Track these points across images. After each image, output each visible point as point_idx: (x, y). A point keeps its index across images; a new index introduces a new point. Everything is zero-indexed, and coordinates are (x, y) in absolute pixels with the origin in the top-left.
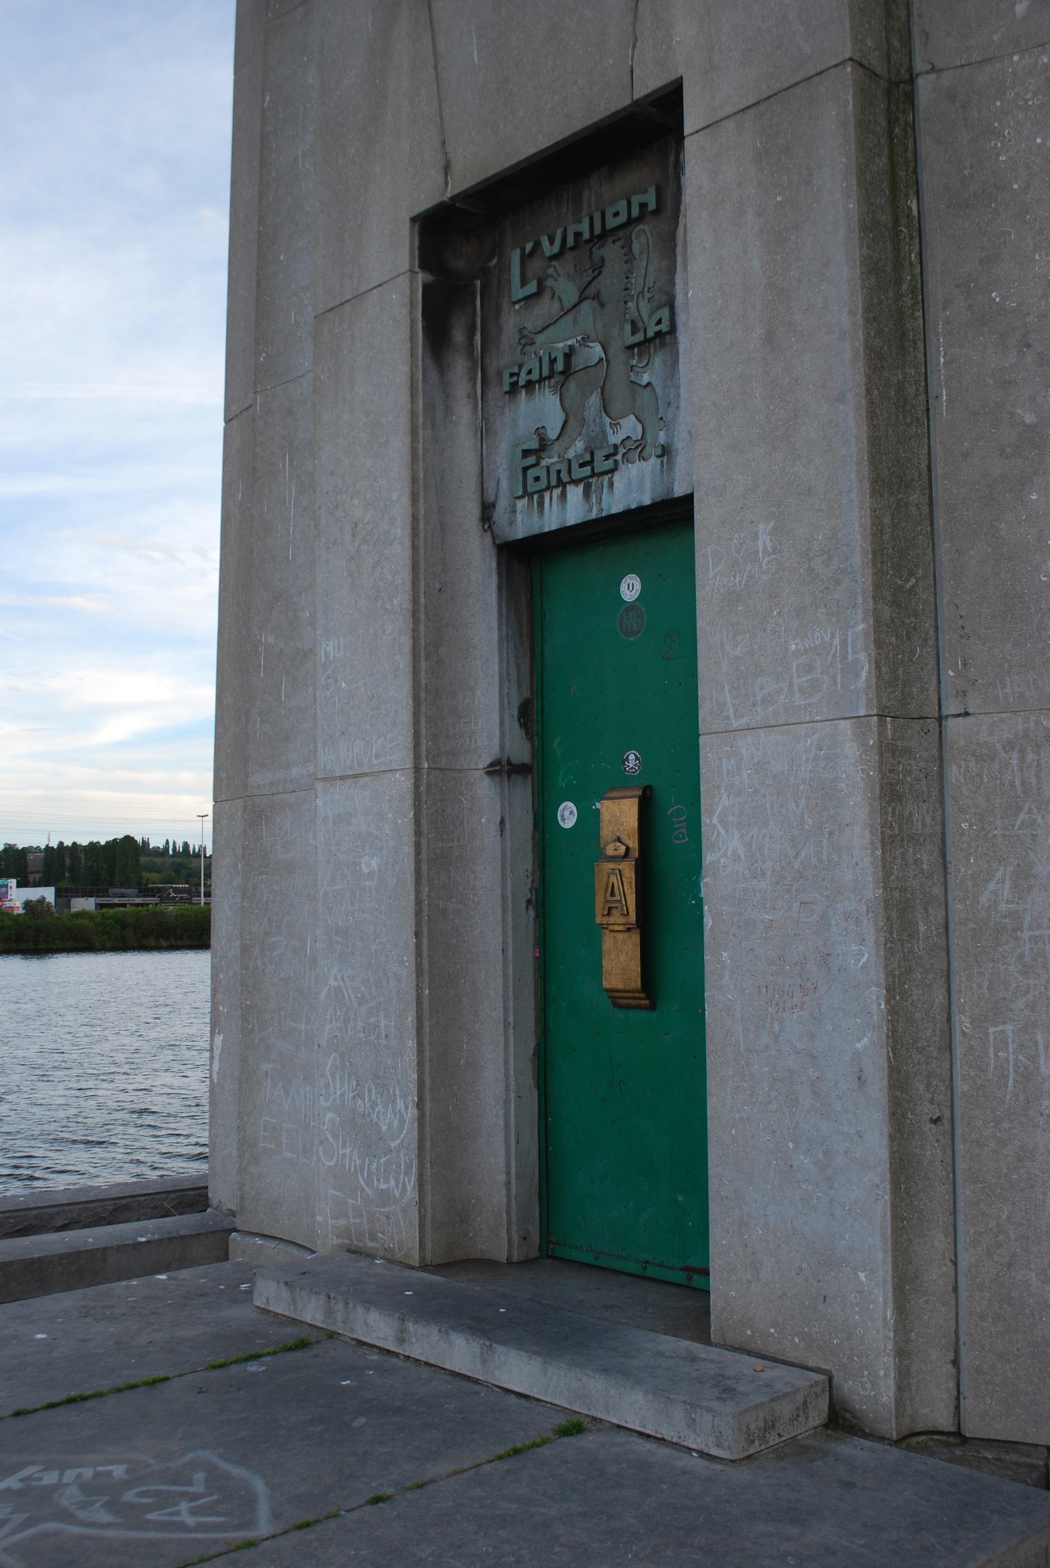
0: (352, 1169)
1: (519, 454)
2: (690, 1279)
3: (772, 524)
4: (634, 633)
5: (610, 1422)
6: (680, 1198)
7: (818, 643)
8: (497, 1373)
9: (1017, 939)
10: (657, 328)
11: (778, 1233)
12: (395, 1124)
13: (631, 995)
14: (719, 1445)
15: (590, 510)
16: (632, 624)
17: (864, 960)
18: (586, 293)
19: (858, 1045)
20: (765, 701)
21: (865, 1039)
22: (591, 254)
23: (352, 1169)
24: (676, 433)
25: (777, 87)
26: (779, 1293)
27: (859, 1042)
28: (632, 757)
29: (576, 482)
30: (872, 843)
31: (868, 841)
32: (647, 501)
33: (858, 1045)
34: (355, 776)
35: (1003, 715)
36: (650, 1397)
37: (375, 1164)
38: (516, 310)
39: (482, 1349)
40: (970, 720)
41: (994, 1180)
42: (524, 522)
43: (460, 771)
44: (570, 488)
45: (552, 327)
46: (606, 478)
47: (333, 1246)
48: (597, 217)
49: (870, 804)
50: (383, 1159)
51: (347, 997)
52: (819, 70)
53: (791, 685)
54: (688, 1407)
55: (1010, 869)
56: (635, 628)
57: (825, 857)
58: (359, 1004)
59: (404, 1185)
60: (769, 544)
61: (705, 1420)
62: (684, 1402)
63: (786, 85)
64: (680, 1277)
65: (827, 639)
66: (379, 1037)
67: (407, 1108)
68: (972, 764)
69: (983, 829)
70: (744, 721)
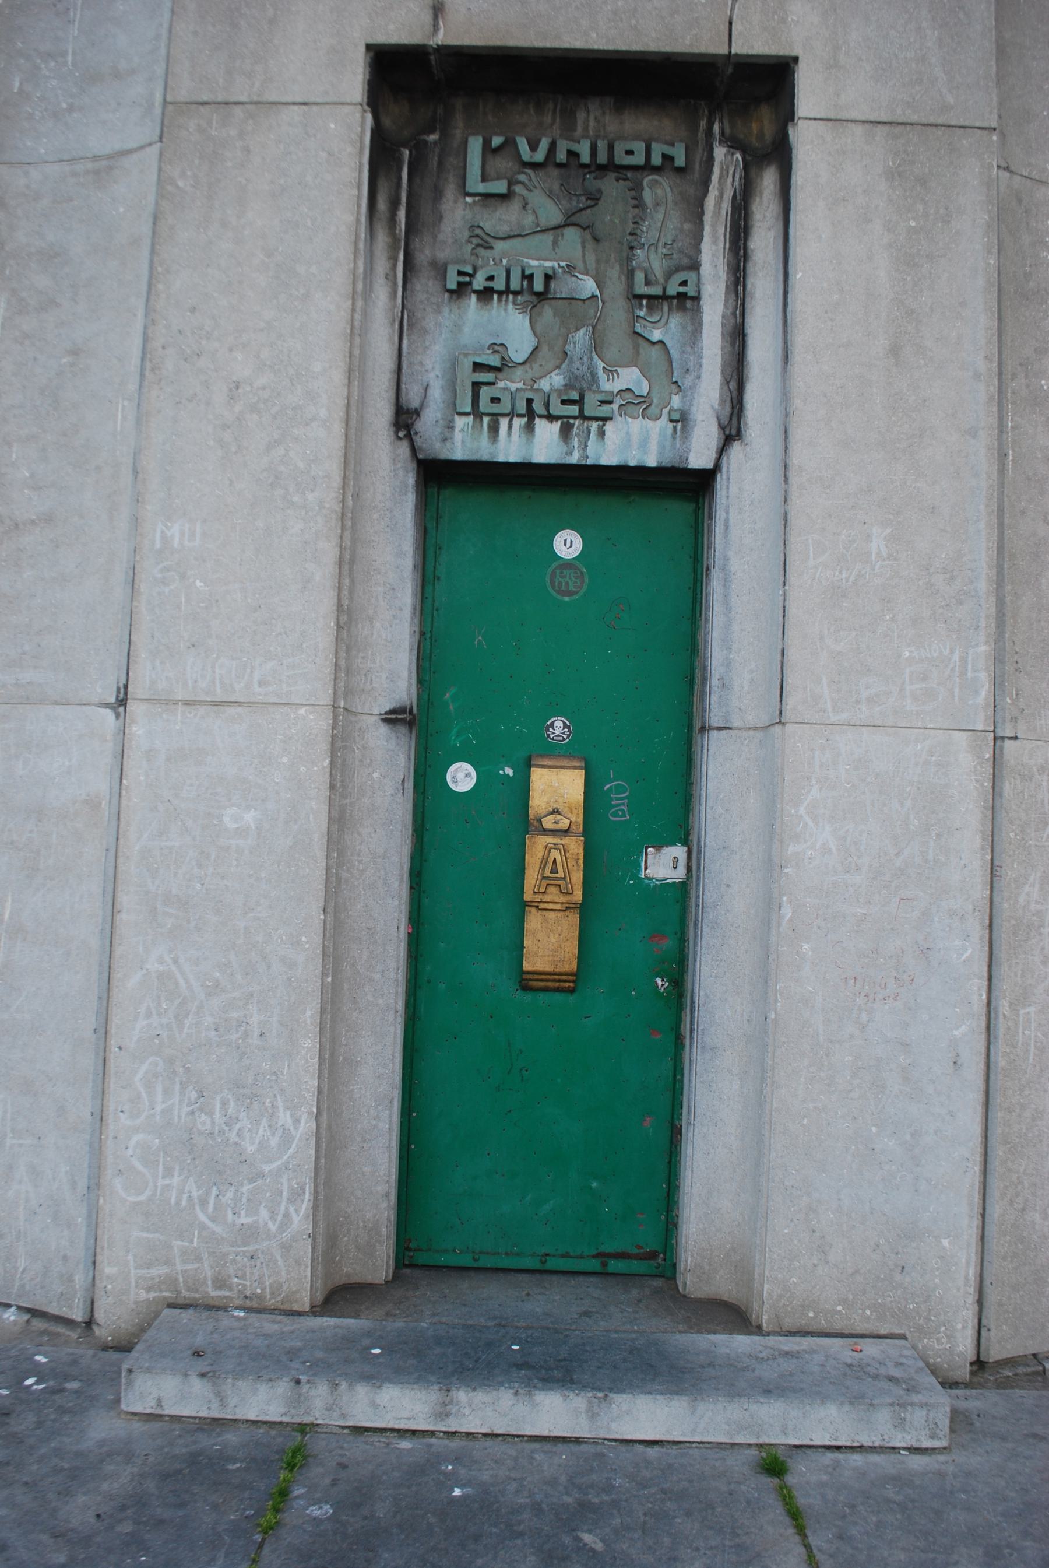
0: (184, 1203)
1: (468, 365)
2: (604, 1265)
3: (889, 531)
4: (570, 593)
5: (785, 1445)
6: (594, 1185)
7: (935, 655)
8: (614, 1426)
9: (1040, 934)
10: (682, 289)
11: (853, 1215)
12: (274, 1142)
13: (556, 977)
14: (932, 1437)
15: (570, 453)
16: (567, 584)
17: (967, 954)
18: (573, 219)
19: (956, 1033)
20: (870, 700)
21: (964, 1027)
22: (584, 180)
23: (184, 1203)
24: (694, 403)
25: (914, 118)
26: (850, 1271)
27: (957, 1029)
28: (559, 724)
29: (551, 418)
30: (983, 848)
31: (979, 846)
32: (652, 462)
33: (956, 1033)
34: (215, 704)
35: (1039, 743)
36: (847, 1407)
37: (230, 1195)
38: (466, 203)
39: (589, 1402)
40: (1018, 742)
41: (1017, 1140)
42: (465, 443)
43: (356, 714)
44: (540, 424)
45: (520, 239)
46: (594, 425)
47: (136, 1303)
48: (602, 145)
49: (982, 812)
50: (245, 1188)
51: (182, 982)
52: (962, 123)
53: (902, 690)
54: (897, 1408)
55: (1039, 874)
56: (571, 588)
57: (931, 856)
58: (209, 995)
59: (287, 1215)
60: (884, 551)
61: (918, 1416)
62: (892, 1405)
63: (925, 121)
64: (595, 1265)
65: (946, 652)
66: (246, 1035)
67: (297, 1121)
68: (1018, 781)
69: (1023, 839)
70: (844, 717)
